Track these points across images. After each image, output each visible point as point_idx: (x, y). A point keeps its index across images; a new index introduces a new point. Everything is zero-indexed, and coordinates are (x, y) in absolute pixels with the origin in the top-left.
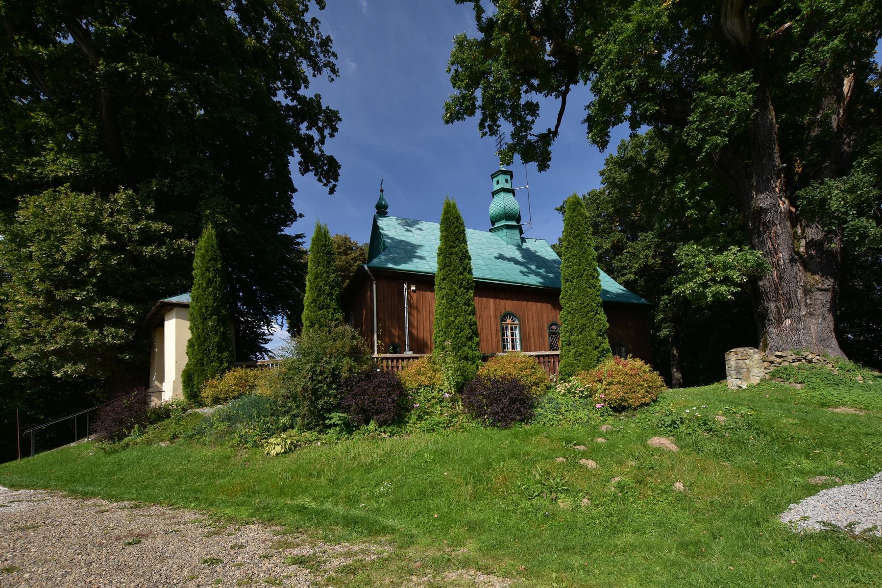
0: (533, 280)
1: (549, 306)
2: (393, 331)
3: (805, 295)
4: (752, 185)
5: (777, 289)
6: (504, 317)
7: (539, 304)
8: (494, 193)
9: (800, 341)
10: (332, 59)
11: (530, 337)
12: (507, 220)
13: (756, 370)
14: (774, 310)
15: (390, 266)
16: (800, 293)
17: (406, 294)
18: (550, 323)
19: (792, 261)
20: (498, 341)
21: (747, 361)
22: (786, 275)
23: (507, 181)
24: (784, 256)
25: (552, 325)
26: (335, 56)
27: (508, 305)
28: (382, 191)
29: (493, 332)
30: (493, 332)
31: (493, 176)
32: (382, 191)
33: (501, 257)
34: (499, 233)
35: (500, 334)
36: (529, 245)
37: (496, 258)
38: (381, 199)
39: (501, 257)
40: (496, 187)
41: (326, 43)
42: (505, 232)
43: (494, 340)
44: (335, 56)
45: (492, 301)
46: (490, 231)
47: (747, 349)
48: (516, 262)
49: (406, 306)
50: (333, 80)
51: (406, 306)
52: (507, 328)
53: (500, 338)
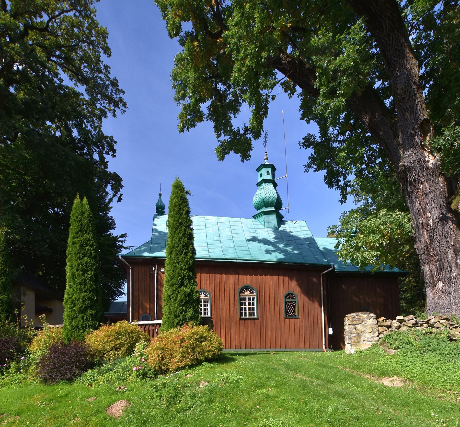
0: (275, 257)
1: (286, 278)
2: (146, 304)
3: (456, 255)
4: (399, 144)
5: (428, 251)
6: (242, 289)
7: (276, 277)
8: (259, 184)
9: (450, 304)
10: (122, 95)
11: (266, 306)
12: (266, 207)
13: (368, 335)
14: (428, 272)
15: (146, 254)
16: (450, 252)
17: (156, 275)
18: (287, 293)
19: (443, 219)
20: (235, 310)
21: (358, 326)
22: (437, 237)
23: (268, 173)
24: (433, 215)
25: (288, 295)
26: (124, 92)
27: (246, 279)
28: (160, 195)
29: (232, 301)
30: (232, 301)
31: (258, 170)
32: (160, 195)
33: (254, 239)
34: (260, 219)
35: (238, 304)
36: (288, 227)
37: (248, 240)
38: (160, 201)
39: (254, 239)
40: (260, 179)
41: (115, 83)
42: (265, 217)
43: (232, 309)
44: (124, 92)
45: (231, 277)
46: (255, 217)
47: (360, 314)
48: (266, 242)
49: (156, 284)
50: (124, 111)
51: (156, 284)
52: (245, 299)
53: (238, 307)
